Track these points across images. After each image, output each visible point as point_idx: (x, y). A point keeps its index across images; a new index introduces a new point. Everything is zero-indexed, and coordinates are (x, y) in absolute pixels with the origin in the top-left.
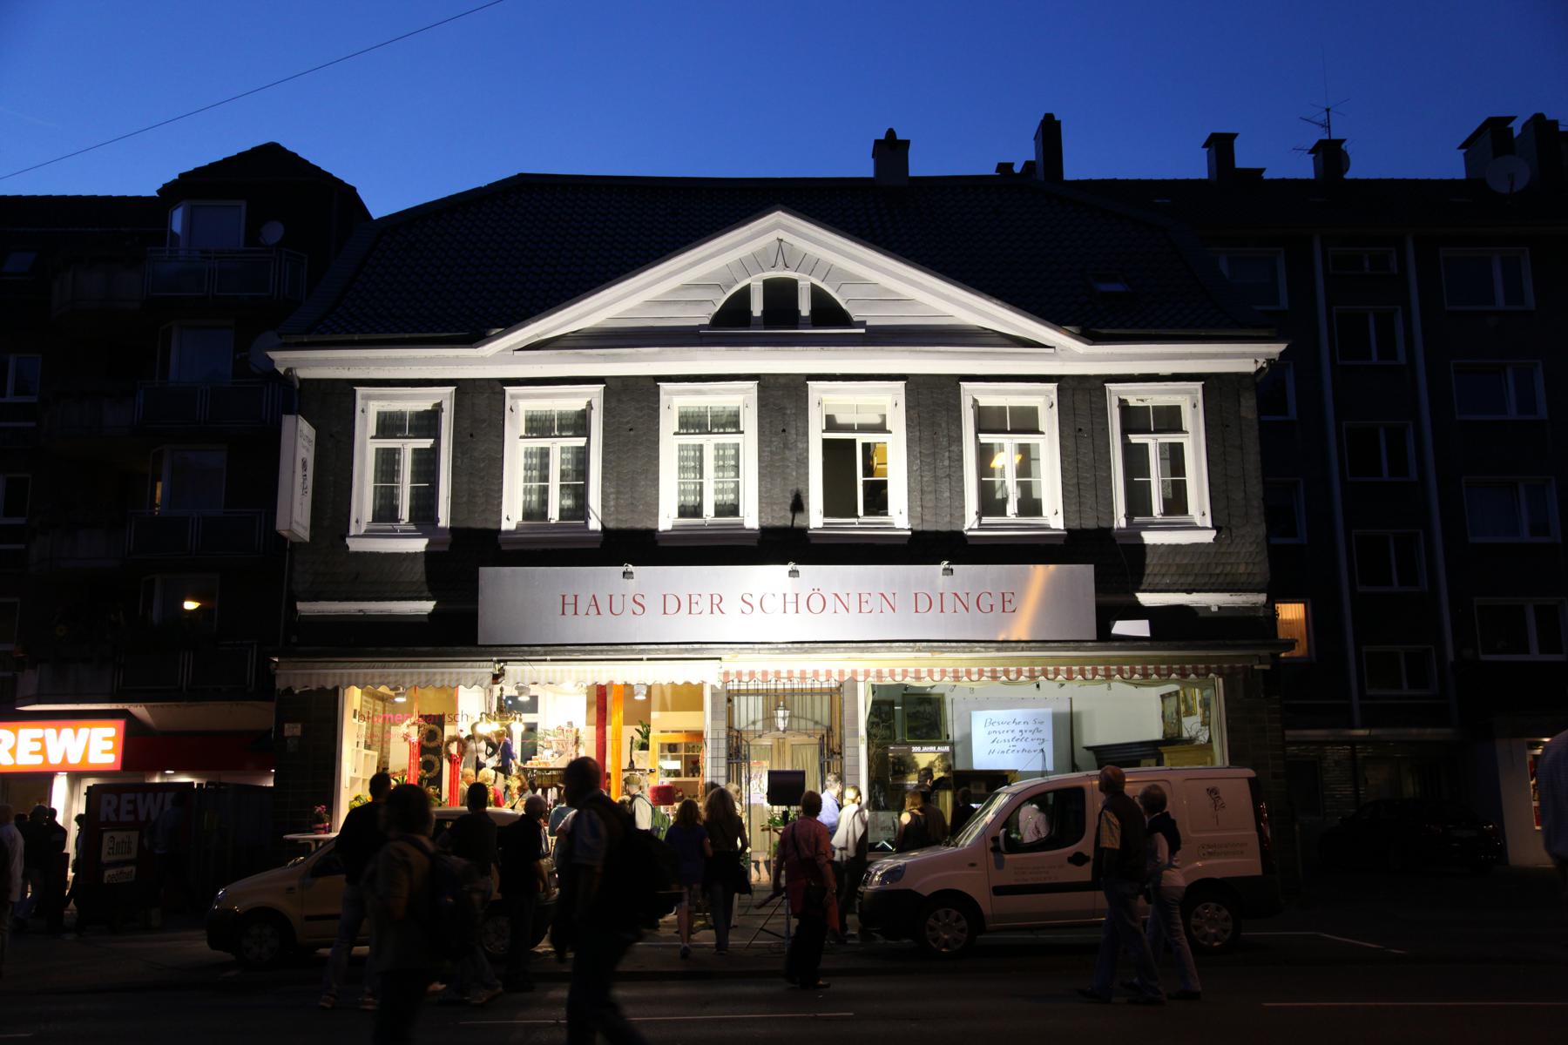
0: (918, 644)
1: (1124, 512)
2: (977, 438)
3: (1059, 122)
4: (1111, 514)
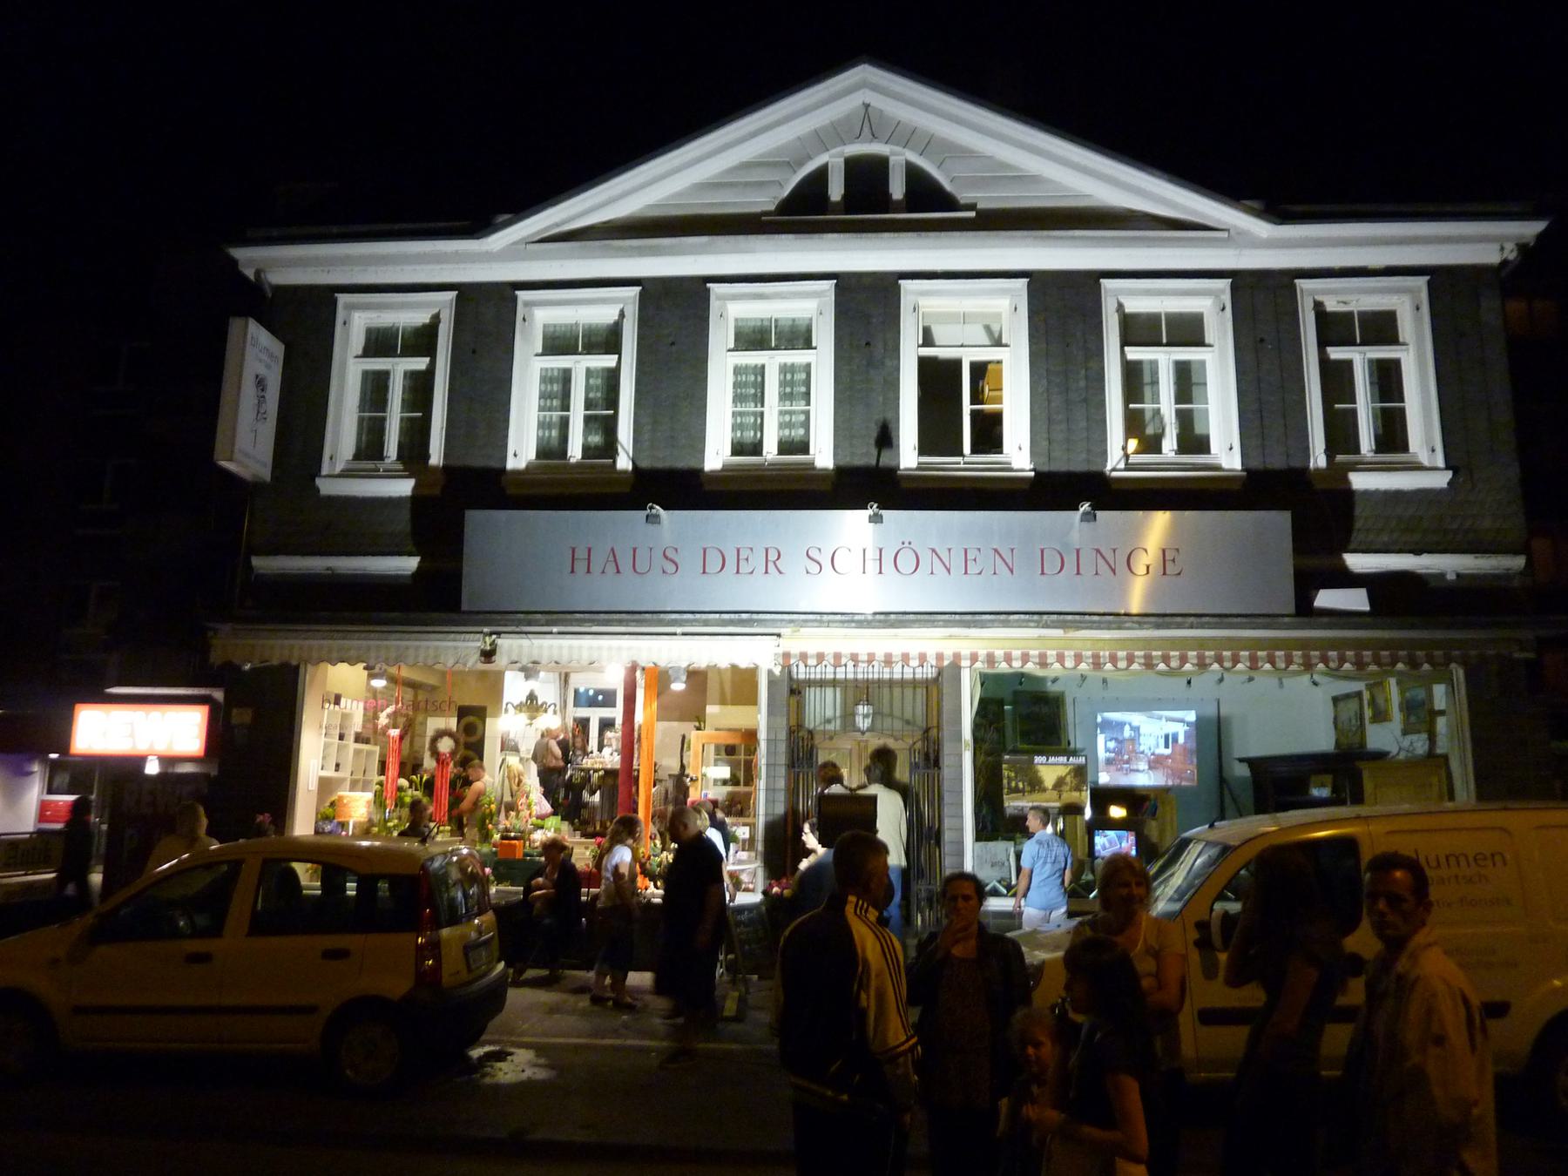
0: (1045, 617)
1: (1324, 447)
2: (1123, 353)
4: (1305, 451)
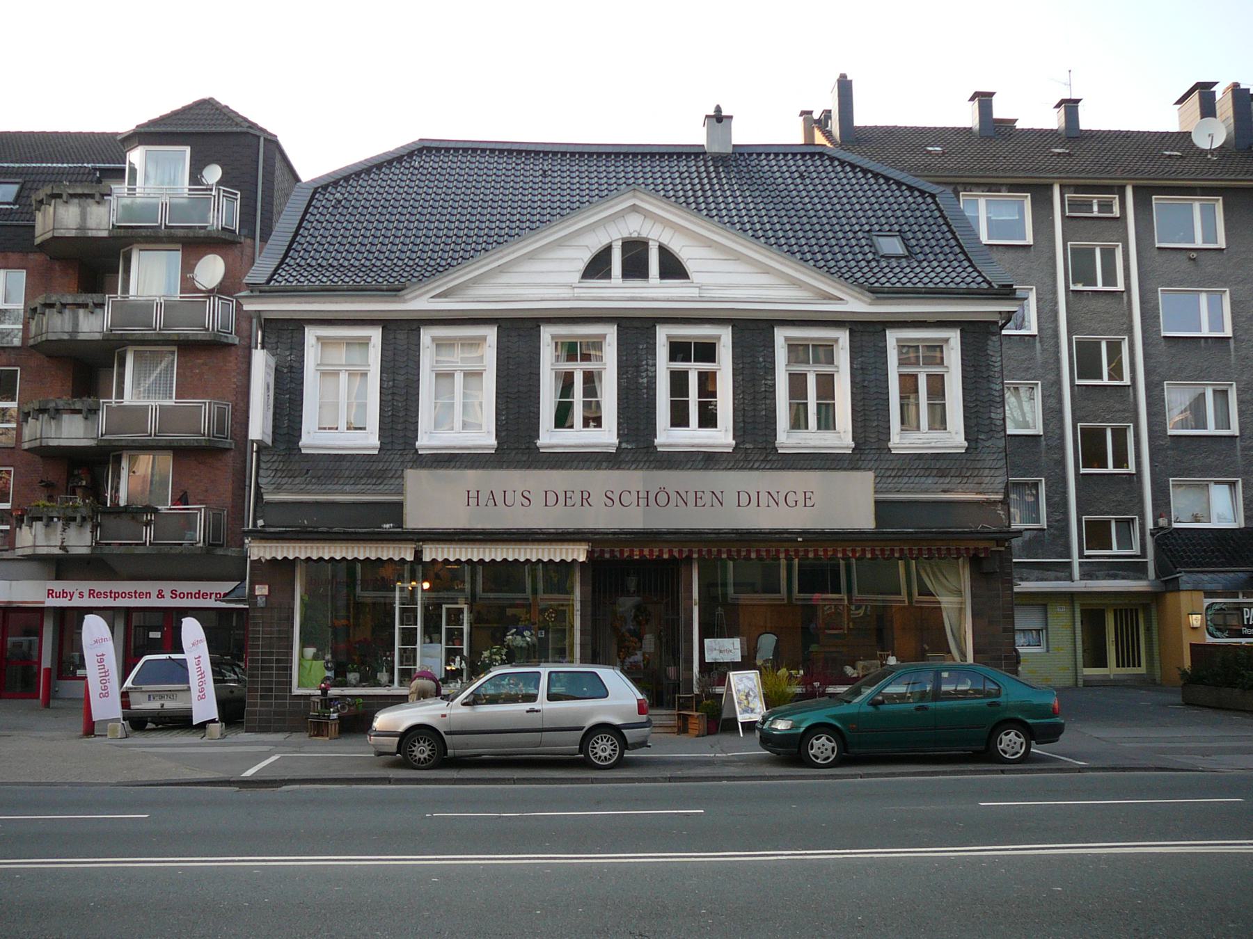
3: (851, 81)
